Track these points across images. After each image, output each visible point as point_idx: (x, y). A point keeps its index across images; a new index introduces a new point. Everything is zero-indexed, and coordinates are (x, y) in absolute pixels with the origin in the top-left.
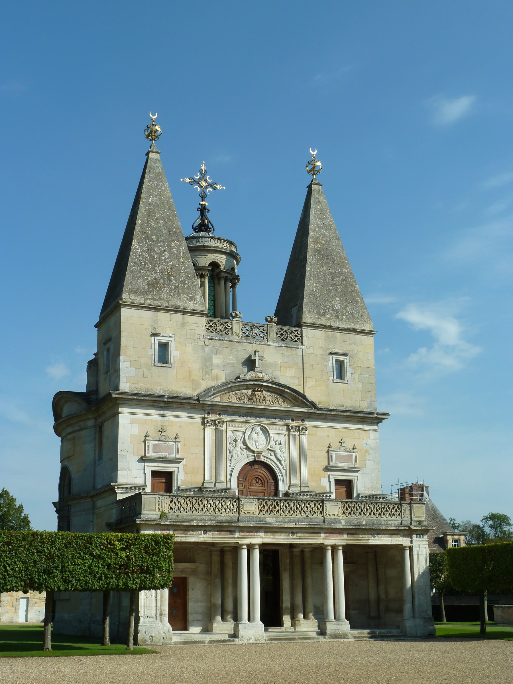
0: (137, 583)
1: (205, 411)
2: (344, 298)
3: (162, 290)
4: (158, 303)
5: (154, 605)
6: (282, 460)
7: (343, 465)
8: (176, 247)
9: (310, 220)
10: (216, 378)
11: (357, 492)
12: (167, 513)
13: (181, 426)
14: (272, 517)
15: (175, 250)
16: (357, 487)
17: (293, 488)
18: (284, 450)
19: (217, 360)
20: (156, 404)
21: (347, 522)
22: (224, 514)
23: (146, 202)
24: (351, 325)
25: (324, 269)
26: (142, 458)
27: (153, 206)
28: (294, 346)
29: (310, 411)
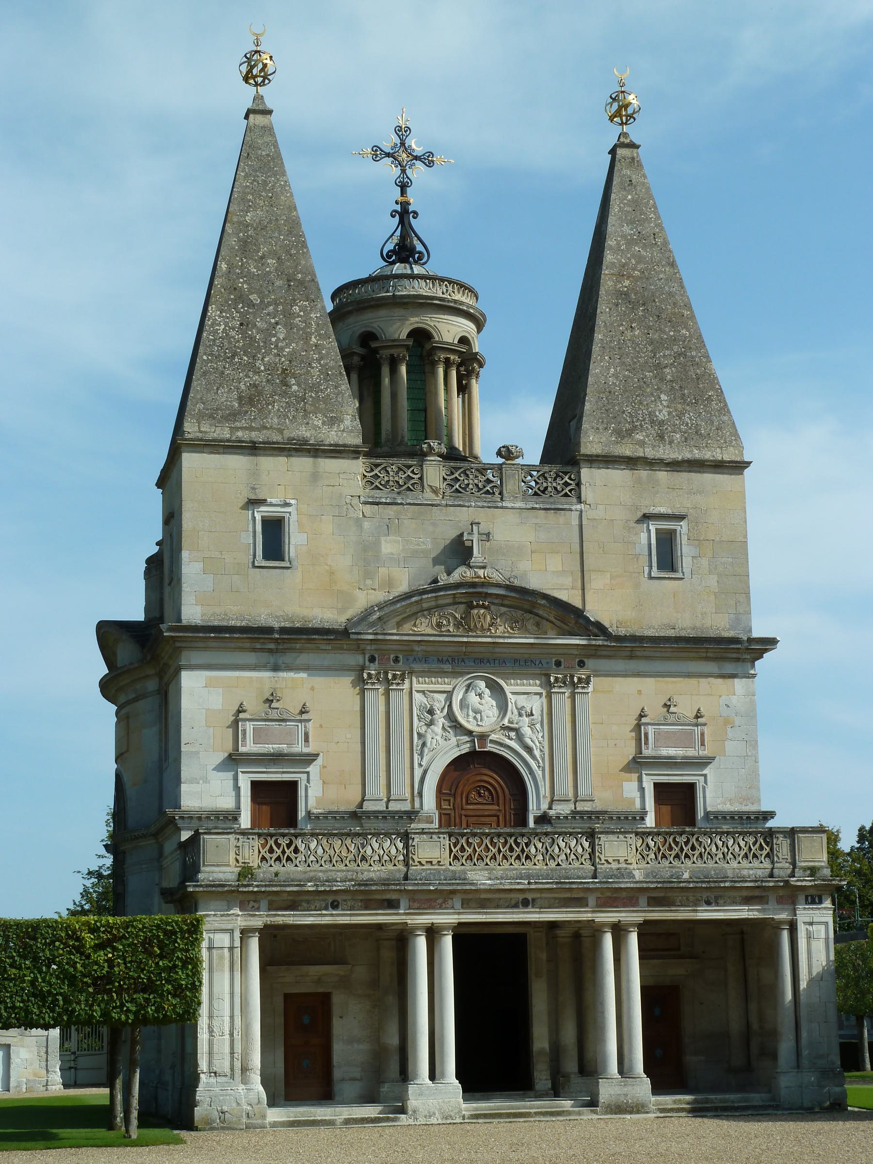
0: (128, 1010)
1: (364, 654)
2: (678, 394)
3: (270, 407)
4: (258, 436)
5: (227, 1050)
6: (534, 748)
7: (672, 752)
8: (302, 313)
9: (609, 227)
10: (390, 583)
11: (705, 809)
12: (255, 869)
13: (313, 687)
14: (480, 870)
15: (300, 321)
16: (704, 797)
17: (558, 804)
18: (538, 726)
19: (389, 546)
20: (258, 646)
21: (647, 875)
22: (376, 867)
23: (240, 223)
24: (691, 451)
25: (636, 333)
26: (230, 755)
27: (255, 229)
28: (561, 507)
29: (594, 643)
